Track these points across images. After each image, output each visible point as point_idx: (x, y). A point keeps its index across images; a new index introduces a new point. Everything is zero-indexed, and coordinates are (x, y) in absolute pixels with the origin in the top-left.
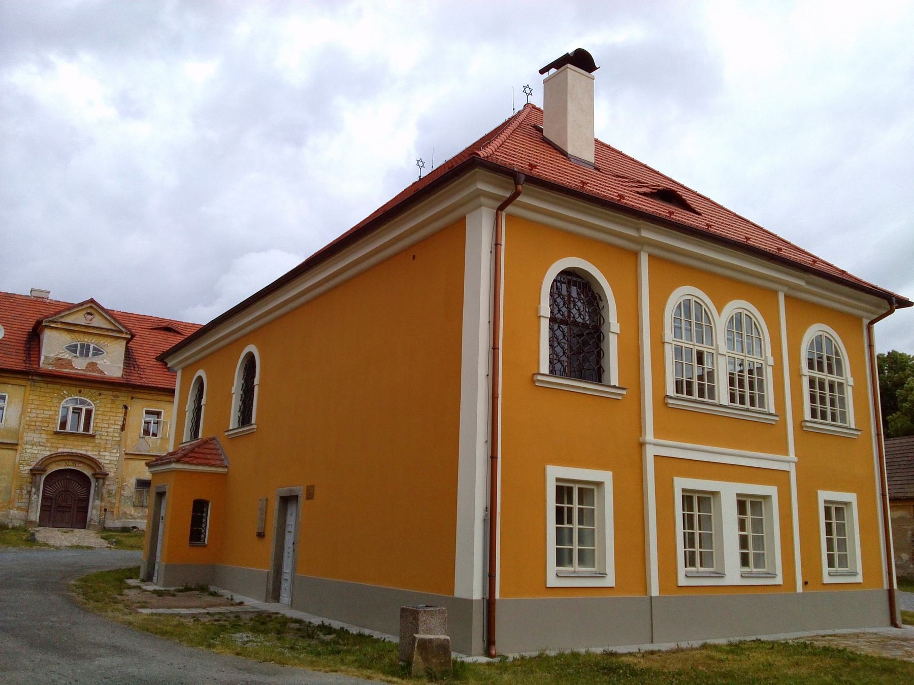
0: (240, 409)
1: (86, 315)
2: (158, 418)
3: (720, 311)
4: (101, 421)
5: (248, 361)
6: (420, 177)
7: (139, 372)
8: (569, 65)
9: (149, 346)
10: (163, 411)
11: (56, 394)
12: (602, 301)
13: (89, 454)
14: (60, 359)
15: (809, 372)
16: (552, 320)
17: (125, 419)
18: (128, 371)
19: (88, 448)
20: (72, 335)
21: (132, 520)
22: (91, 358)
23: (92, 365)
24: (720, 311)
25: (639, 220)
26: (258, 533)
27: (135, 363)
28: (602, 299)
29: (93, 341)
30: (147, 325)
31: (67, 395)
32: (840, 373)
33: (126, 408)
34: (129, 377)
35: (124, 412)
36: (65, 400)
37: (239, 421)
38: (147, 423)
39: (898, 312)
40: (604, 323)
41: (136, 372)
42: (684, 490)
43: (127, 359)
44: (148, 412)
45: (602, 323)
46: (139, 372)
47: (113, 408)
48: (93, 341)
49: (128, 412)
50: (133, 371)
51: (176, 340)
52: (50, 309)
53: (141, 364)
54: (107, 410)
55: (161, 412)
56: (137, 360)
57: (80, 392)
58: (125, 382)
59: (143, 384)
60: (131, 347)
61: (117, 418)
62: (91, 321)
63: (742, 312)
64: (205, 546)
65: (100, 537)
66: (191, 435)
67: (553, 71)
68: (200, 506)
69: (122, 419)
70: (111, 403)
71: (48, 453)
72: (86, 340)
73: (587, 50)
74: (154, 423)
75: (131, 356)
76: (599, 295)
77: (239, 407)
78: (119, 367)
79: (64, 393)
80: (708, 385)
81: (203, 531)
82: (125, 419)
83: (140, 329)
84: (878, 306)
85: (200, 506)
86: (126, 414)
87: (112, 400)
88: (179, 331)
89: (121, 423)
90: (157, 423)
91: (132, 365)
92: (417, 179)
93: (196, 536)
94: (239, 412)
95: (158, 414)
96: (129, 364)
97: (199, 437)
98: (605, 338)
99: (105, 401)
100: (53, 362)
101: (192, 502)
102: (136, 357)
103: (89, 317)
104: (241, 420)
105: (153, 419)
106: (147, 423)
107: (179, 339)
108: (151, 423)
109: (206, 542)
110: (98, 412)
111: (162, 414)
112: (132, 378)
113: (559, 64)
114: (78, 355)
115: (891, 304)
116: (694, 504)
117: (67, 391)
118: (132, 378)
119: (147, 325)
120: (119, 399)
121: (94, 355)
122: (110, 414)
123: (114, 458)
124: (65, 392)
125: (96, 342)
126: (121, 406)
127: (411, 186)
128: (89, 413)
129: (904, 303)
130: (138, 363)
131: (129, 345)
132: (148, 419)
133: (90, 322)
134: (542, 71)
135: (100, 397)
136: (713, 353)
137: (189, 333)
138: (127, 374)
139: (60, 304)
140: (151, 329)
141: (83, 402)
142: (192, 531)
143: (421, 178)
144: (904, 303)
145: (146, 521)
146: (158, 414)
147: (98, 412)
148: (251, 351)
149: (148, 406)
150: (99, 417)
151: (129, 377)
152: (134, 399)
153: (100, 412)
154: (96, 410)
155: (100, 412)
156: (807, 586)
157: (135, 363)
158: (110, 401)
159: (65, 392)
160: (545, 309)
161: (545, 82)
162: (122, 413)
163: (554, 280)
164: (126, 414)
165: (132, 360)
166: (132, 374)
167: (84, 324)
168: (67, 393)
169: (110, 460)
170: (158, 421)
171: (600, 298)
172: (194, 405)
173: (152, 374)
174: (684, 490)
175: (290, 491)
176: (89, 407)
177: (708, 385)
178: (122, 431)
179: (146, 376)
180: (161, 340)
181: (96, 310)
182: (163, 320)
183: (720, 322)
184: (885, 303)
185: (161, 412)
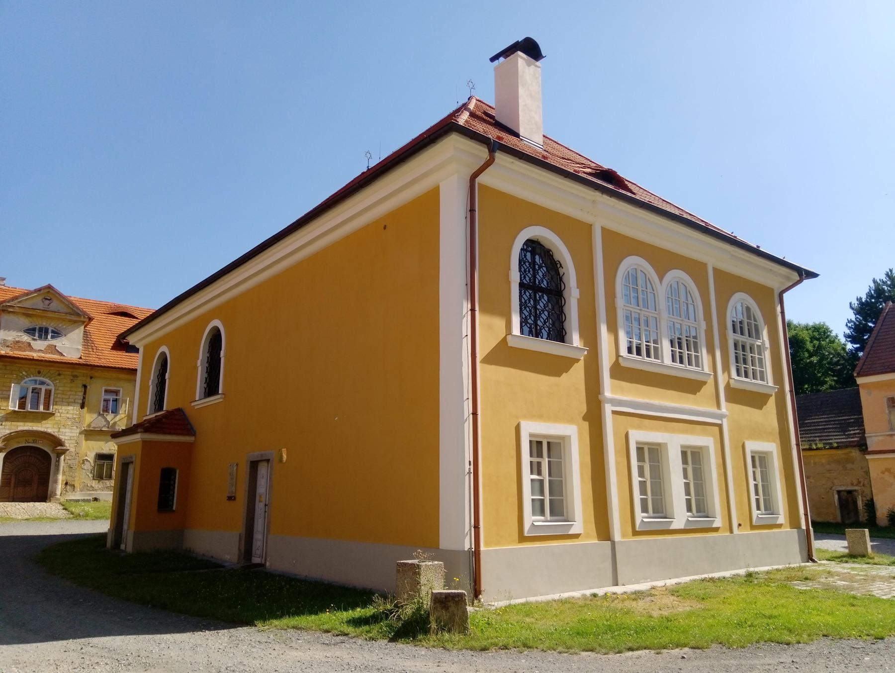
0: (206, 380)
1: (43, 300)
2: (117, 396)
3: (661, 280)
4: (61, 400)
5: (213, 336)
6: (368, 167)
7: (97, 354)
8: (519, 53)
9: (106, 329)
10: (121, 389)
11: (15, 376)
12: (563, 268)
13: (49, 431)
14: (18, 342)
15: (734, 335)
16: (522, 285)
17: (84, 398)
18: (86, 352)
19: (48, 426)
20: (31, 319)
21: (93, 492)
22: (51, 342)
23: (53, 349)
24: (661, 280)
25: (595, 192)
26: (228, 497)
27: (93, 345)
28: (563, 266)
29: (52, 325)
30: (104, 310)
31: (26, 376)
32: (758, 337)
33: (85, 387)
34: (87, 358)
35: (83, 391)
36: (30, 379)
37: (205, 391)
38: (106, 401)
39: (807, 283)
40: (565, 289)
41: (94, 353)
42: (637, 443)
43: (86, 341)
44: (106, 391)
45: (563, 288)
46: (97, 354)
47: (72, 387)
48: (52, 325)
49: (87, 391)
50: (91, 353)
51: (132, 323)
52: (6, 295)
53: (99, 346)
54: (66, 389)
55: (119, 390)
56: (95, 342)
57: (39, 372)
58: (84, 363)
59: (101, 364)
60: (89, 330)
61: (77, 397)
62: (48, 305)
63: (678, 280)
64: (174, 511)
65: (102, 502)
66: (155, 408)
67: (502, 59)
68: (167, 475)
69: (82, 398)
70: (71, 383)
71: (8, 432)
72: (44, 324)
73: (534, 39)
74: (113, 401)
75: (89, 339)
76: (560, 263)
77: (205, 379)
78: (78, 349)
79: (23, 374)
80: (654, 346)
81: (171, 498)
82: (84, 398)
83: (97, 314)
84: (788, 278)
85: (167, 475)
86: (85, 393)
87: (71, 380)
88: (135, 315)
89: (81, 401)
90: (116, 400)
91: (90, 347)
92: (365, 170)
93: (164, 503)
94: (205, 383)
95: (116, 392)
96: (88, 345)
97: (164, 410)
98: (566, 304)
99: (65, 381)
100: (11, 344)
101: (561, 377)
102: (94, 340)
103: (47, 302)
104: (207, 391)
105: (111, 397)
106: (106, 401)
107: (135, 322)
108: (110, 400)
109: (174, 508)
110: (58, 392)
111: (121, 392)
112: (91, 359)
113: (508, 52)
114: (36, 337)
115: (800, 275)
116: (645, 454)
117: (26, 372)
118: (91, 359)
119: (104, 310)
120: (78, 378)
121: (53, 337)
122: (69, 393)
123: (75, 435)
124: (24, 373)
125: (55, 326)
126: (80, 386)
127: (360, 175)
128: (48, 393)
129: (811, 275)
130: (96, 345)
131: (86, 328)
132: (108, 397)
133: (49, 307)
134: (493, 59)
135: (59, 377)
136: (656, 318)
137: (142, 317)
138: (86, 355)
139: (17, 290)
140: (108, 314)
141: (42, 383)
142: (160, 499)
143: (369, 168)
144: (811, 275)
145: (112, 492)
146: (116, 392)
147: (58, 392)
148: (218, 326)
149: (108, 385)
150: (59, 396)
151: (87, 358)
152: (93, 379)
153: (60, 392)
154: (55, 390)
155: (60, 392)
156: (740, 527)
157: (93, 345)
158: (69, 381)
159: (24, 373)
160: (515, 277)
161: (496, 69)
162: (82, 392)
163: (522, 249)
164: (85, 393)
165: (91, 342)
166: (90, 355)
167: (42, 308)
168: (25, 374)
169: (71, 437)
170: (117, 399)
171: (561, 265)
172: (157, 380)
173: (111, 355)
174: (637, 443)
175: (262, 455)
176: (49, 388)
177: (654, 346)
178: (82, 409)
179: (104, 357)
180: (118, 324)
181: (53, 294)
182: (118, 307)
183: (661, 290)
184: (796, 276)
185: (119, 390)
